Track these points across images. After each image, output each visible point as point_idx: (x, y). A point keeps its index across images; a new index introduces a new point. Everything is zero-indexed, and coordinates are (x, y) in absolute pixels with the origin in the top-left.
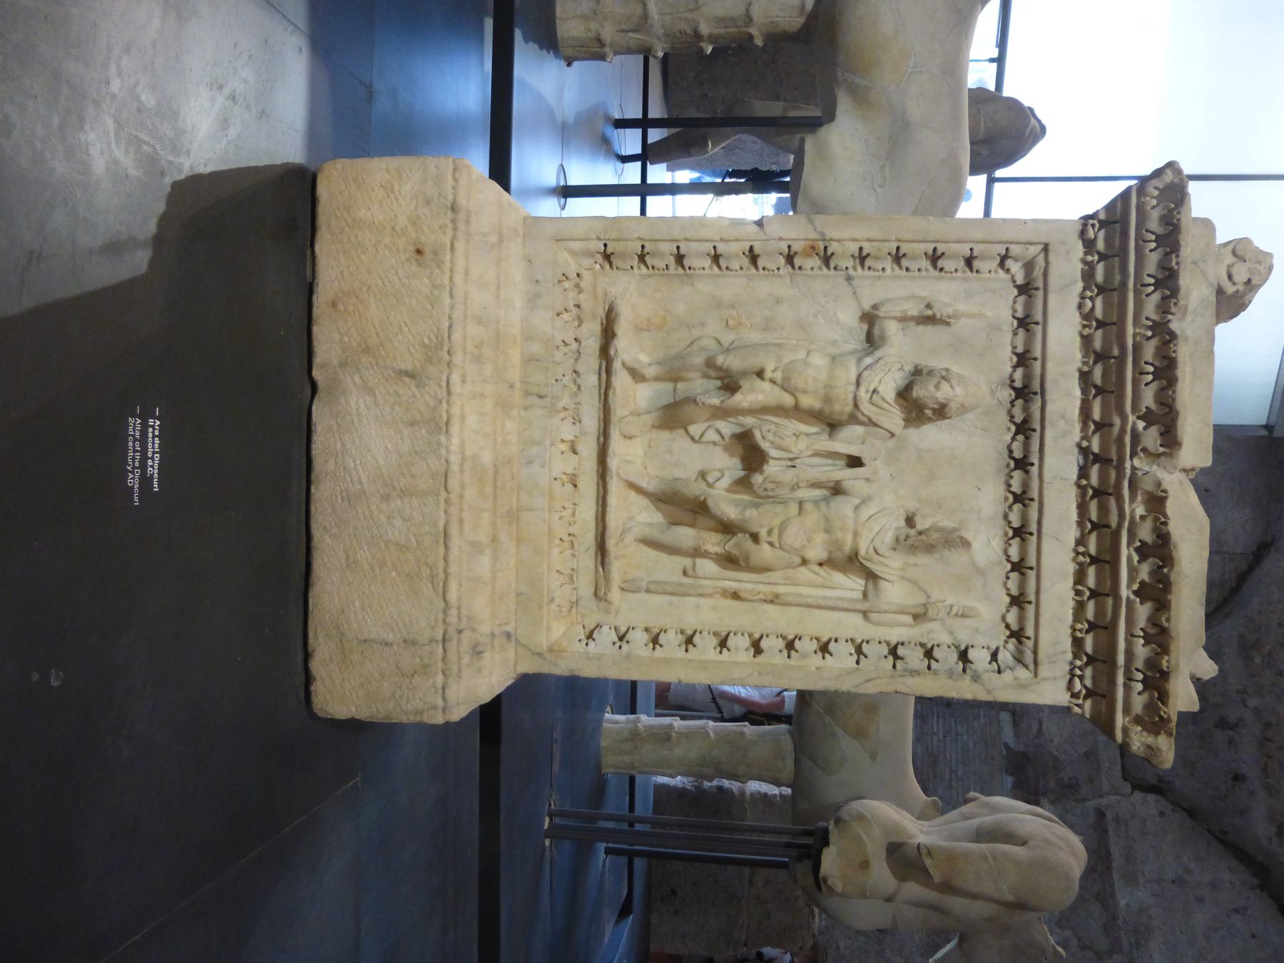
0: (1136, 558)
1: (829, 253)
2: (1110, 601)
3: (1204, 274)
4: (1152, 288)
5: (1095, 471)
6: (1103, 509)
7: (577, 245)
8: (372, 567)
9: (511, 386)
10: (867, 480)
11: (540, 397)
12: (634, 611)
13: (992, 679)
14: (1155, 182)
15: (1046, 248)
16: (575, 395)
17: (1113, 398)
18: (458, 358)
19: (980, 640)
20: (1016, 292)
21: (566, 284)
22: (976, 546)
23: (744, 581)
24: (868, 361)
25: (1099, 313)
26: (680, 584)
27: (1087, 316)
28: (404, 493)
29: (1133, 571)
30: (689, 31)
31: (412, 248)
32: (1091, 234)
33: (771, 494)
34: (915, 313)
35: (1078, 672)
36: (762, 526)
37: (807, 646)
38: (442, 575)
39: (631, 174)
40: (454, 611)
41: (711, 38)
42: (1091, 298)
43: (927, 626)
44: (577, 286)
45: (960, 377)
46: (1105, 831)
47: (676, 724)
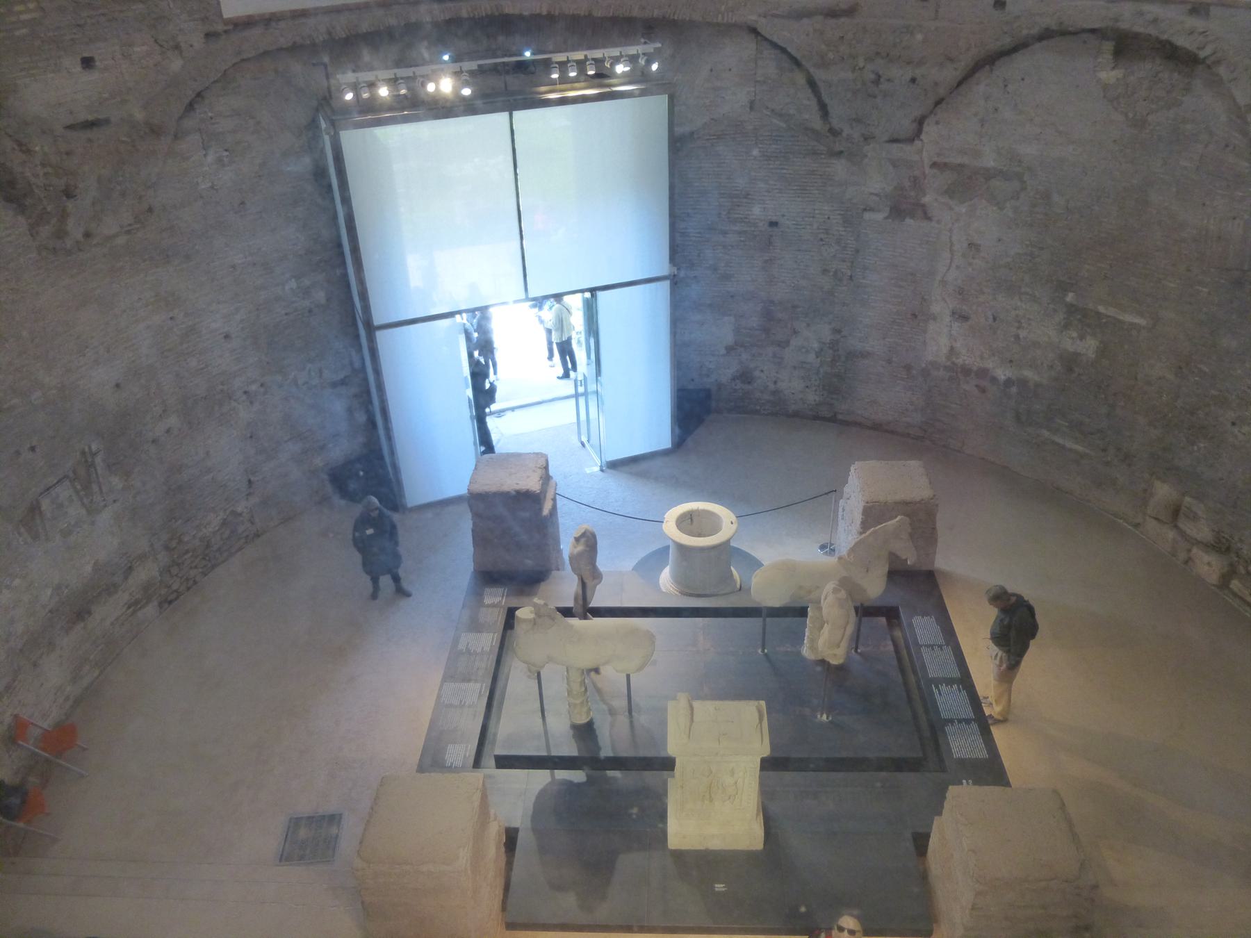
46: (945, 164)
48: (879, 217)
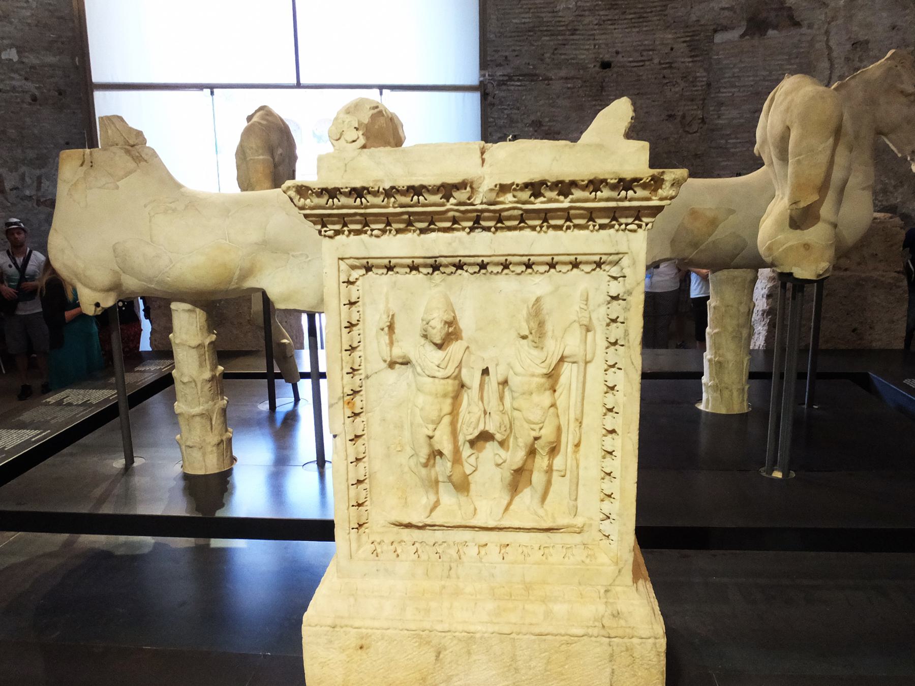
0: (542, 199)
1: (351, 392)
2: (572, 212)
3: (353, 159)
4: (363, 199)
5: (484, 224)
6: (510, 218)
7: (354, 545)
8: (562, 680)
9: (444, 587)
10: (497, 365)
11: (451, 569)
12: (590, 507)
13: (630, 282)
14: (296, 201)
15: (342, 259)
16: (449, 545)
17: (436, 217)
18: (427, 625)
19: (604, 287)
20: (370, 273)
21: (379, 550)
22: (539, 293)
23: (568, 440)
24: (419, 369)
25: (381, 226)
26: (571, 481)
27: (384, 231)
28: (514, 659)
29: (550, 201)
30: (209, 385)
31: (360, 651)
32: (331, 233)
33: (508, 426)
34: (387, 337)
35: (623, 227)
36: (529, 435)
37: (610, 401)
38: (566, 638)
39: (305, 386)
40: (590, 631)
41: (214, 368)
42: (372, 230)
43: (595, 321)
44: (379, 543)
45: (426, 312)
47: (709, 357)
48: (734, 35)
